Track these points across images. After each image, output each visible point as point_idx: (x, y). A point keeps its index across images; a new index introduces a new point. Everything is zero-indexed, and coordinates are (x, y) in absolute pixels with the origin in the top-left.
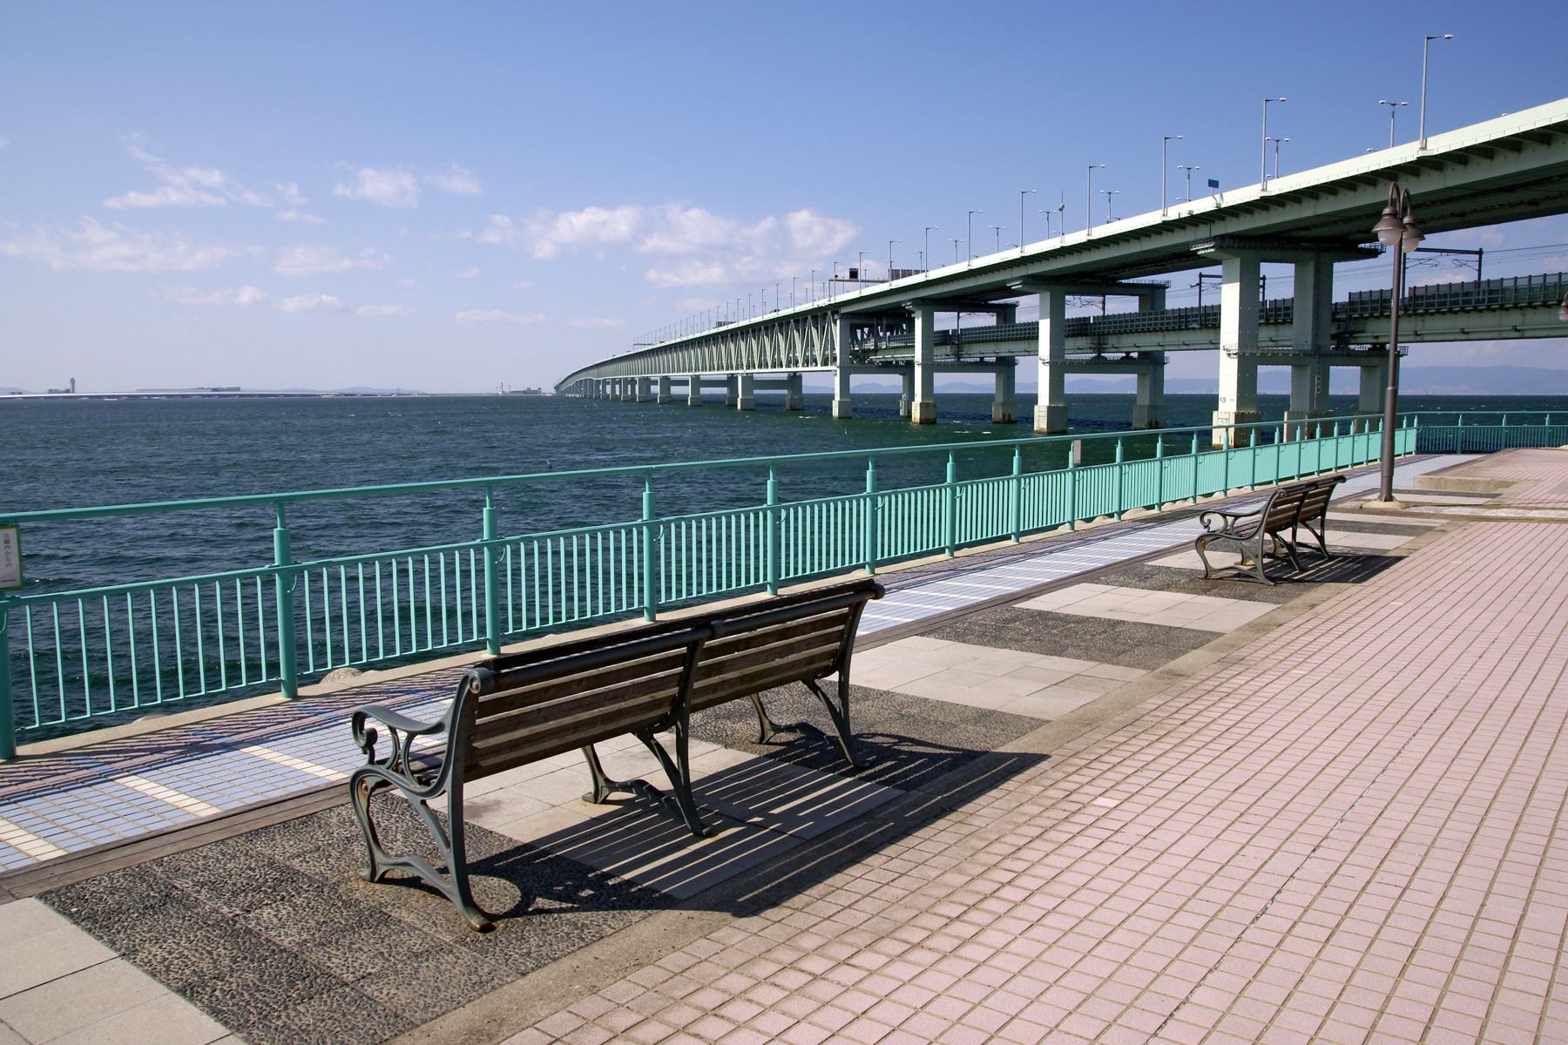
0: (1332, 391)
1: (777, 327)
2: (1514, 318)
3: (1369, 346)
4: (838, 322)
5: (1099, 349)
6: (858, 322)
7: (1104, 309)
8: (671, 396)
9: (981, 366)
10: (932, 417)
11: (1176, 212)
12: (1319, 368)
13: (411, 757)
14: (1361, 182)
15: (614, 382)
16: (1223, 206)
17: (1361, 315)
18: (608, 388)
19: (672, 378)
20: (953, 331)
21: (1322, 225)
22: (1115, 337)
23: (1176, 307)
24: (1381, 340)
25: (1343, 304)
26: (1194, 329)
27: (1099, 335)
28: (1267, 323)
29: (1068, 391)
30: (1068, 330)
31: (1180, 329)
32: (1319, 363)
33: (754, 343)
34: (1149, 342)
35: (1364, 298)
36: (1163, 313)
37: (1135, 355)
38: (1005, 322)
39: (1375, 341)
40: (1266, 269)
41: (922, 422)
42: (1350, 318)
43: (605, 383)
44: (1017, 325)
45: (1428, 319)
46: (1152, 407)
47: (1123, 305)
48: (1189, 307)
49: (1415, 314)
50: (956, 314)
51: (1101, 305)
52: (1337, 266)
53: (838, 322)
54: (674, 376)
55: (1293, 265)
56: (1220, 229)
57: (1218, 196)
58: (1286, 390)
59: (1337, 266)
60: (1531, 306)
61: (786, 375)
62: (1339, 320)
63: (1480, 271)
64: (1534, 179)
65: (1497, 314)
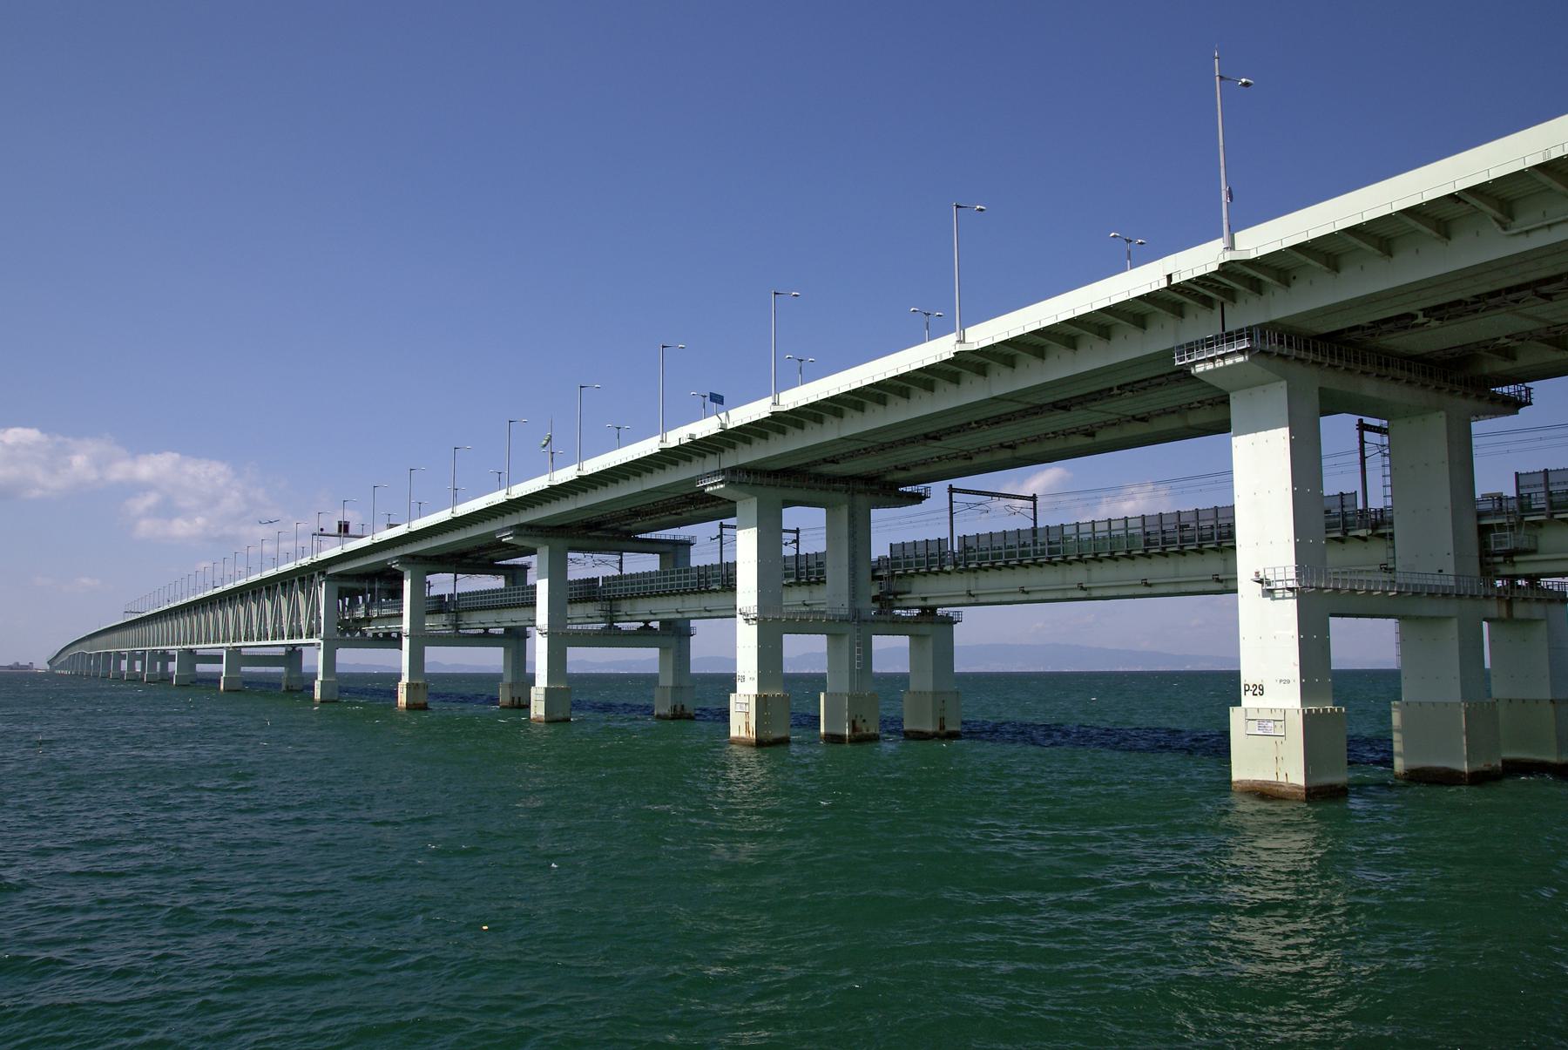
0: (876, 669)
1: (297, 584)
2: (1077, 574)
3: (917, 611)
4: (324, 585)
5: (611, 618)
7: (621, 570)
8: (196, 674)
9: (485, 638)
10: (421, 700)
11: (676, 437)
12: (858, 637)
14: (809, 419)
15: (133, 657)
16: (730, 426)
17: (1007, 562)
18: (124, 665)
19: (199, 652)
20: (451, 596)
21: (852, 455)
22: (628, 602)
23: (702, 565)
24: (930, 603)
25: (885, 559)
26: (715, 591)
27: (609, 599)
28: (798, 584)
29: (571, 669)
30: (571, 595)
31: (702, 592)
32: (859, 631)
33: (254, 607)
34: (668, 608)
35: (921, 551)
36: (686, 571)
37: (655, 625)
38: (514, 584)
39: (922, 603)
40: (792, 517)
41: (408, 706)
42: (893, 575)
43: (120, 656)
45: (982, 575)
46: (677, 688)
47: (643, 563)
48: (709, 564)
49: (967, 569)
51: (618, 566)
52: (876, 514)
53: (324, 585)
54: (202, 648)
55: (824, 510)
56: (731, 459)
57: (723, 415)
58: (821, 667)
59: (876, 514)
60: (1097, 559)
61: (283, 649)
62: (880, 578)
63: (798, 549)
64: (956, 423)
65: (1171, 560)
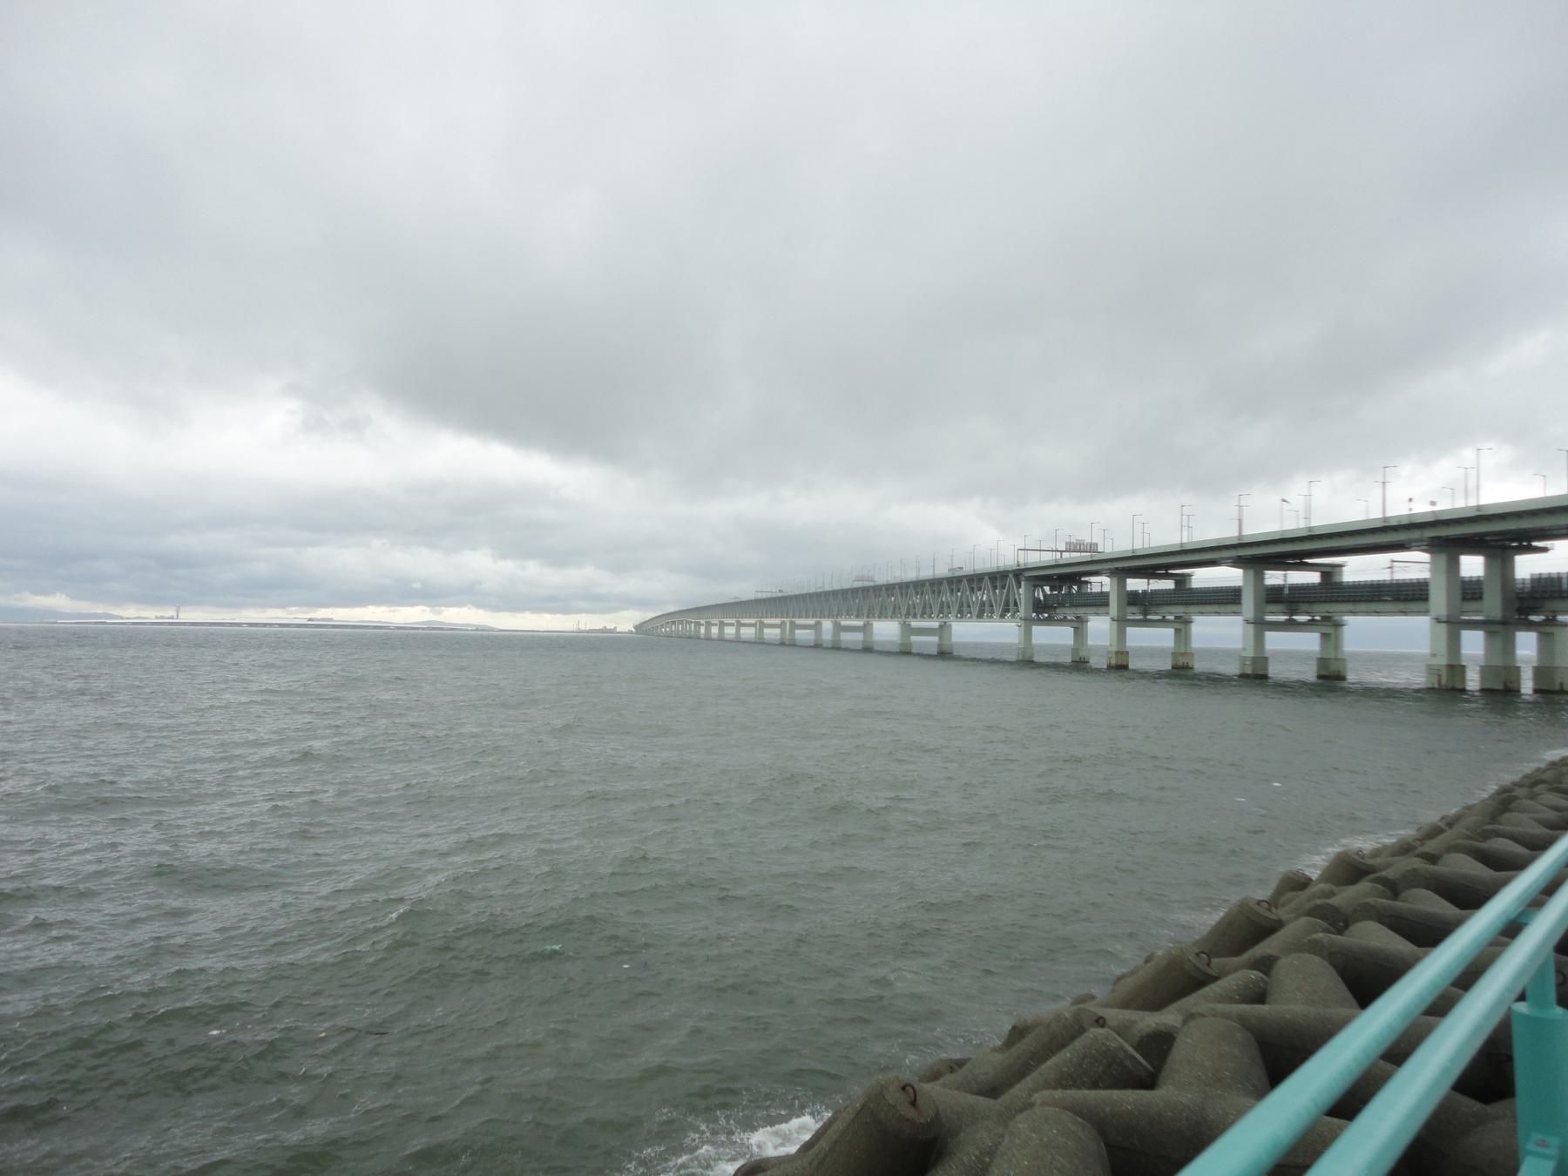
6: (1037, 583)
13: (771, 1100)
44: (1185, 590)
50: (1146, 580)
